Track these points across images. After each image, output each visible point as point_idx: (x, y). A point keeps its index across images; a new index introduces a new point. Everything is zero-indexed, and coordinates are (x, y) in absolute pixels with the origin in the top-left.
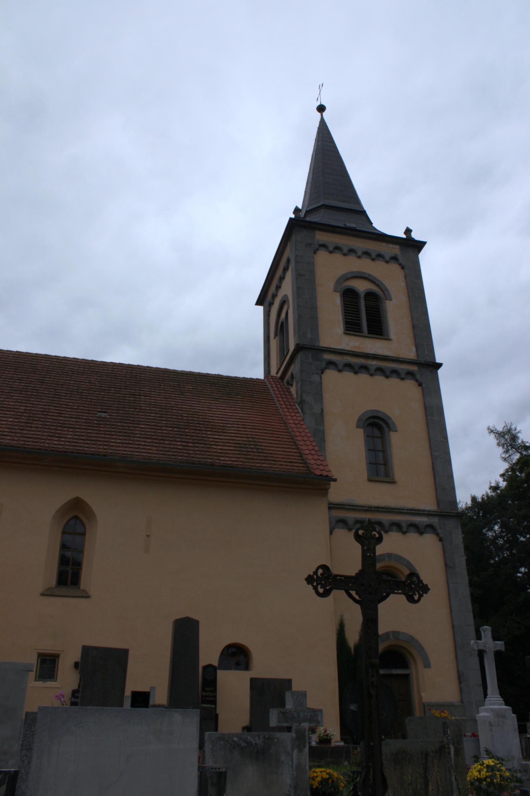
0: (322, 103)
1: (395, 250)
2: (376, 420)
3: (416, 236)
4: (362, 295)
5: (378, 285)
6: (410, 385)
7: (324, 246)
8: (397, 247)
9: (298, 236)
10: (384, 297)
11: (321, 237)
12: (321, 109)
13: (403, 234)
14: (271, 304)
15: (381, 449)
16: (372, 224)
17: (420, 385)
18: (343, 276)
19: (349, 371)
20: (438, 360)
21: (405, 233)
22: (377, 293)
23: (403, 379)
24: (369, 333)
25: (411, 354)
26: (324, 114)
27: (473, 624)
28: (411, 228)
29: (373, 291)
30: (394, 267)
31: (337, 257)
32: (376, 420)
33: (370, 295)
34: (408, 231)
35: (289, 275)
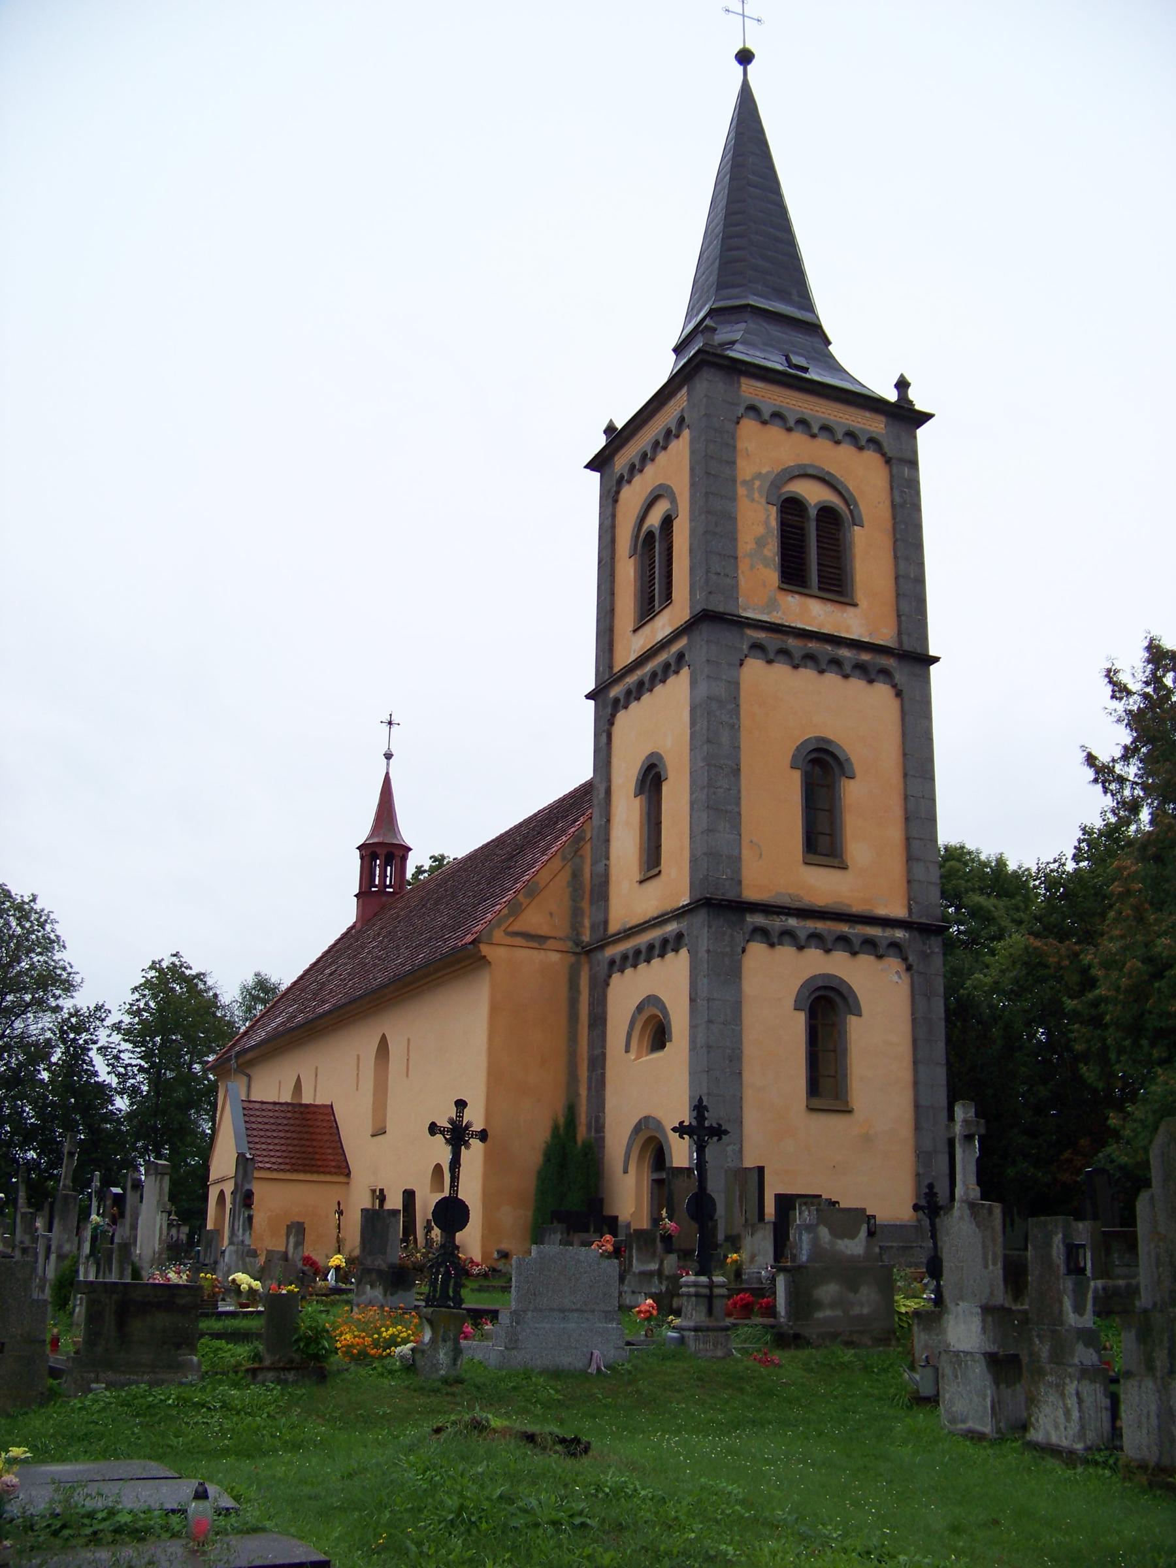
0: (747, 46)
1: (875, 425)
2: (832, 994)
3: (920, 400)
4: (813, 513)
5: (840, 494)
6: (882, 692)
7: (753, 409)
8: (883, 419)
9: (707, 383)
10: (849, 515)
11: (751, 389)
12: (745, 57)
13: (893, 387)
14: (621, 481)
15: (828, 832)
16: (829, 343)
17: (899, 694)
18: (784, 471)
19: (784, 663)
20: (932, 652)
21: (898, 386)
22: (844, 516)
23: (846, 677)
24: (820, 589)
25: (885, 635)
26: (749, 67)
27: (945, 1083)
28: (909, 378)
29: (833, 506)
30: (871, 458)
31: (775, 432)
32: (832, 994)
33: (827, 513)
34: (902, 385)
35: (681, 447)
